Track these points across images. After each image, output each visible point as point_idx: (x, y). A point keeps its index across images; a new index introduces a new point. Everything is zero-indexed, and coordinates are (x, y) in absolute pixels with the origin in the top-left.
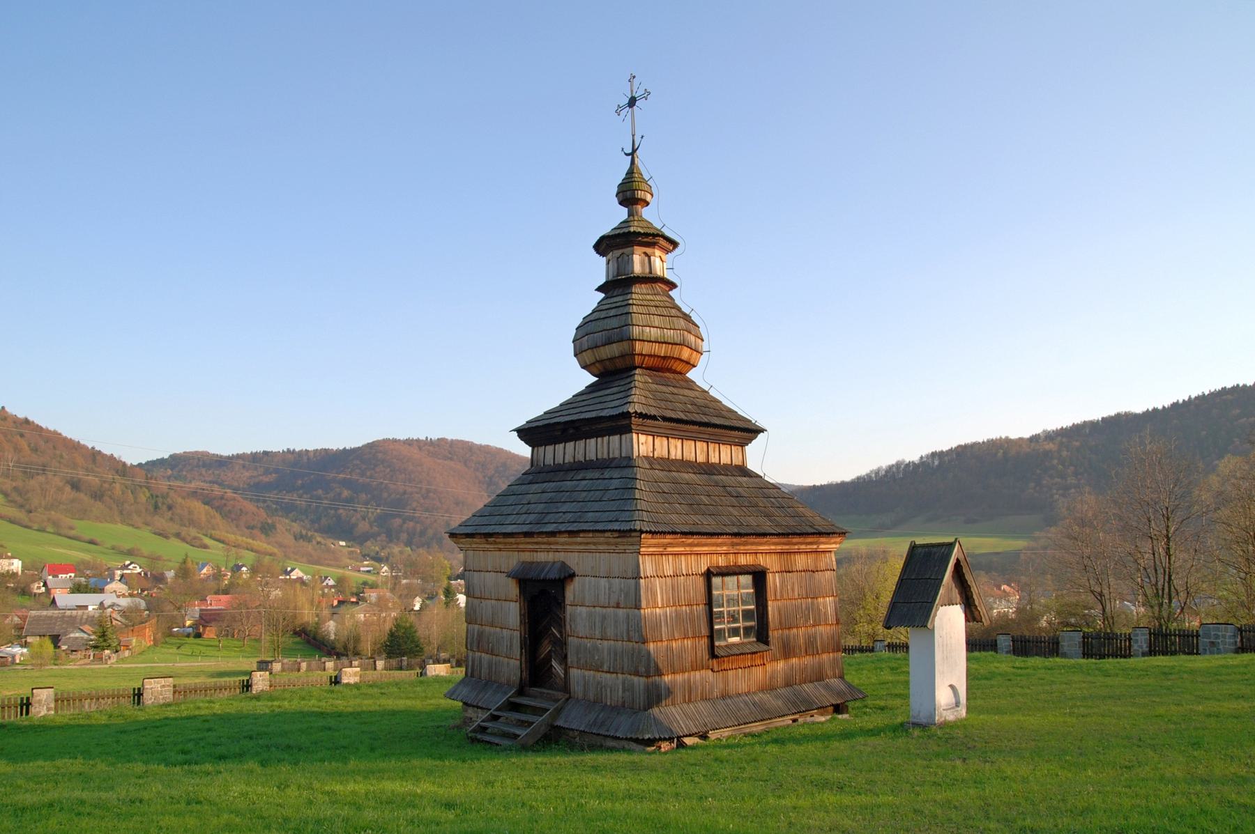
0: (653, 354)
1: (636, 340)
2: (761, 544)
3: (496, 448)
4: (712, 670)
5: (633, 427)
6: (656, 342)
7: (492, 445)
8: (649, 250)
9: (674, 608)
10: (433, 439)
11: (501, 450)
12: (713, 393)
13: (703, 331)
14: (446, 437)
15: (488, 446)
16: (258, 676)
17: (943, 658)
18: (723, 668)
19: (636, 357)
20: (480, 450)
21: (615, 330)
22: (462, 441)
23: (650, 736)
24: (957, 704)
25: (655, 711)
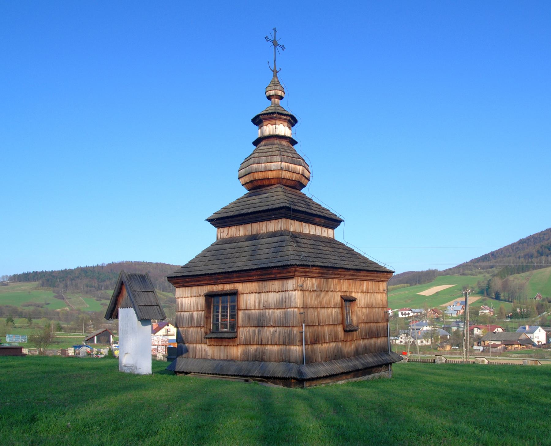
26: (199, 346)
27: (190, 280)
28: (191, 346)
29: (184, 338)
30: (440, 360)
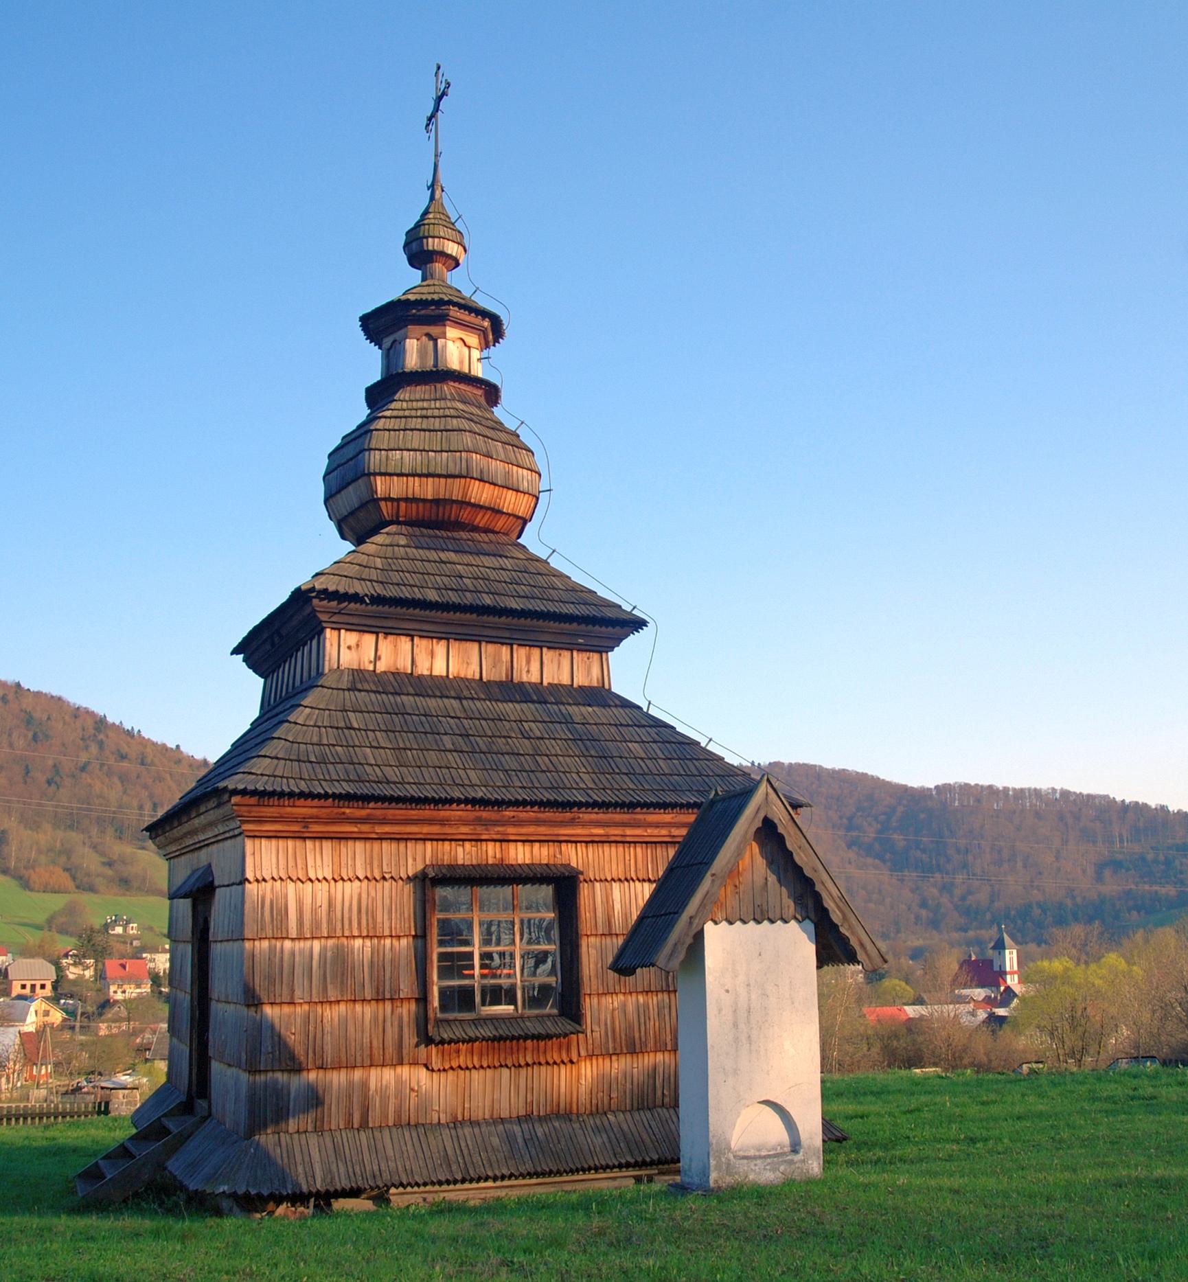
0: (410, 496)
1: (375, 474)
2: (562, 824)
3: (857, 773)
4: (426, 1066)
5: (323, 617)
6: (413, 475)
7: (850, 769)
8: (434, 330)
9: (331, 942)
10: (762, 764)
11: (865, 775)
12: (556, 563)
13: (540, 462)
14: (782, 761)
15: (844, 770)
16: (121, 1096)
17: (736, 1040)
18: (455, 1065)
19: (382, 504)
20: (833, 778)
21: (350, 463)
22: (805, 765)
23: (226, 1188)
24: (795, 1146)
25: (266, 1139)
26: (383, 1078)
27: (364, 813)
28: (337, 1079)
29: (299, 1051)
30: (127, 1104)
